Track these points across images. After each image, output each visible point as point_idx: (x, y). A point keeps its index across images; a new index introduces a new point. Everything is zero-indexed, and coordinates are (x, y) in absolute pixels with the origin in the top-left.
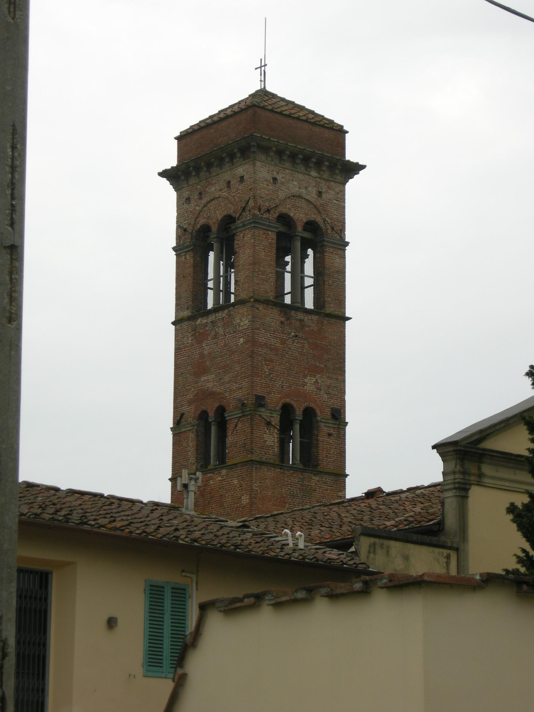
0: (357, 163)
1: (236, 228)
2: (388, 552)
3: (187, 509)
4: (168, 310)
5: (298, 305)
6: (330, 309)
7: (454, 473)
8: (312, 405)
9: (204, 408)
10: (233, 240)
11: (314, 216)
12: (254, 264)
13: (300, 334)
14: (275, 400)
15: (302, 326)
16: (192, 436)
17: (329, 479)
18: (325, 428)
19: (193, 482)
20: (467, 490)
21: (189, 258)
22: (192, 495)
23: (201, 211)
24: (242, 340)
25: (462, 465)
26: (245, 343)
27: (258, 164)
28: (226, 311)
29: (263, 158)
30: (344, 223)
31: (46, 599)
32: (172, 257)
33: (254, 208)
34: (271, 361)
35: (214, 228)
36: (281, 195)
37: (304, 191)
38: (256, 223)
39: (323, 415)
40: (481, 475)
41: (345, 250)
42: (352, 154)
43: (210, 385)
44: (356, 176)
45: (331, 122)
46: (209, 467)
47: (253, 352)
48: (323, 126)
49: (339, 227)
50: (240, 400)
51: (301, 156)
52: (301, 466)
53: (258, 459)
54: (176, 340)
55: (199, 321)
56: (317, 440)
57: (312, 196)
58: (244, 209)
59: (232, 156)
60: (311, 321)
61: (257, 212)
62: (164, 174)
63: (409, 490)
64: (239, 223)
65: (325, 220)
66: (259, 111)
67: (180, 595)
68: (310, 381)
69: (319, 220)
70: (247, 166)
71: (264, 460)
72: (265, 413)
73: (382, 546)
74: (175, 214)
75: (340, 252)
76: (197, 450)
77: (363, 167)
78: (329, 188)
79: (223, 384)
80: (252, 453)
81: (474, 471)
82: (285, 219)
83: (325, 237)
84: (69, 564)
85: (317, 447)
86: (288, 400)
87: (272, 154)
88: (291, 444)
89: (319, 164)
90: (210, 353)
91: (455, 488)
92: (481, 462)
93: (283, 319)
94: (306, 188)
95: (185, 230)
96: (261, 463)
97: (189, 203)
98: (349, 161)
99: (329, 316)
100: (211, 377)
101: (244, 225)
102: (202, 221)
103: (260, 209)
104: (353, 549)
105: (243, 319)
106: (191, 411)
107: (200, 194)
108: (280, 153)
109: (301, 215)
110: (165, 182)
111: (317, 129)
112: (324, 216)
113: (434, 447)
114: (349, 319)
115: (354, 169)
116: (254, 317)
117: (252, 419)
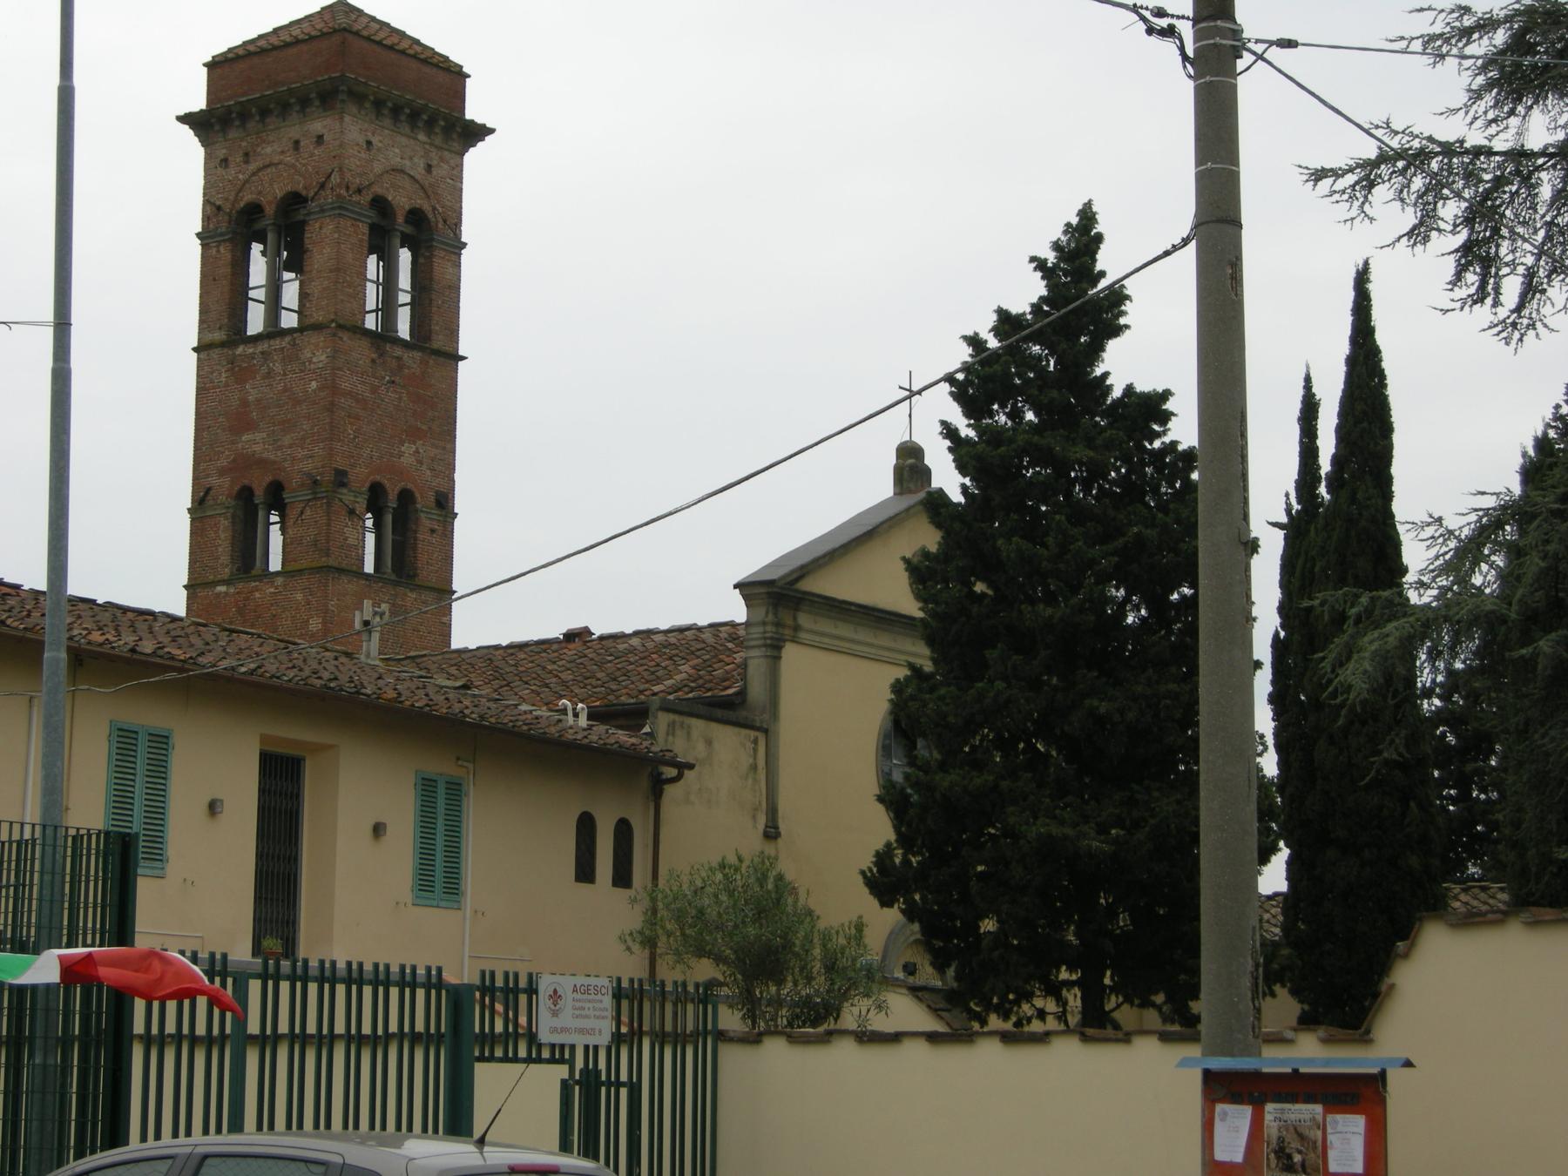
0: (484, 126)
1: (309, 214)
2: (689, 734)
3: (368, 656)
4: (187, 328)
5: (386, 335)
6: (438, 342)
7: (764, 624)
8: (410, 486)
9: (246, 482)
10: (303, 232)
11: (421, 202)
12: (338, 270)
13: (397, 379)
14: (361, 476)
15: (401, 367)
16: (225, 523)
17: (429, 596)
18: (427, 520)
19: (378, 619)
20: (779, 648)
21: (225, 252)
22: (376, 636)
23: (246, 181)
24: (314, 384)
25: (775, 614)
26: (320, 389)
27: (347, 119)
28: (287, 339)
29: (354, 110)
30: (461, 214)
31: (298, 796)
32: (196, 247)
33: (339, 185)
34: (358, 418)
35: (270, 210)
36: (378, 168)
37: (407, 163)
38: (341, 209)
39: (424, 501)
40: (797, 628)
41: (460, 255)
42: (474, 111)
43: (257, 448)
44: (480, 144)
45: (446, 59)
46: (253, 572)
47: (332, 403)
48: (436, 66)
49: (454, 221)
50: (309, 475)
51: (407, 111)
52: (393, 577)
53: (335, 564)
54: (198, 376)
55: (240, 350)
56: (416, 539)
57: (419, 171)
58: (322, 186)
59: (305, 103)
60: (412, 358)
61: (343, 192)
62: (186, 119)
63: (637, 633)
64: (313, 205)
65: (434, 209)
66: (350, 37)
67: (455, 791)
68: (408, 449)
69: (427, 207)
70: (328, 121)
71: (344, 566)
72: (347, 496)
73: (682, 725)
74: (202, 182)
75: (453, 257)
76: (233, 544)
77: (492, 131)
78: (442, 159)
79: (280, 448)
80: (328, 555)
81: (790, 622)
82: (381, 205)
83: (430, 233)
84: (331, 747)
85: (415, 549)
86: (378, 478)
87: (367, 105)
88: (370, 539)
89: (430, 124)
90: (258, 400)
91: (765, 645)
92: (797, 609)
93: (374, 356)
94: (411, 158)
95: (219, 208)
96: (341, 571)
97: (227, 167)
98: (472, 121)
99: (438, 353)
100: (259, 436)
101: (323, 211)
102: (248, 197)
103: (348, 188)
104: (647, 729)
105: (317, 353)
106: (224, 486)
107: (247, 154)
108: (378, 104)
109: (402, 199)
110: (186, 130)
111: (427, 70)
112: (434, 202)
113: (736, 587)
114: (463, 358)
115: (477, 133)
116: (336, 351)
117: (329, 504)
